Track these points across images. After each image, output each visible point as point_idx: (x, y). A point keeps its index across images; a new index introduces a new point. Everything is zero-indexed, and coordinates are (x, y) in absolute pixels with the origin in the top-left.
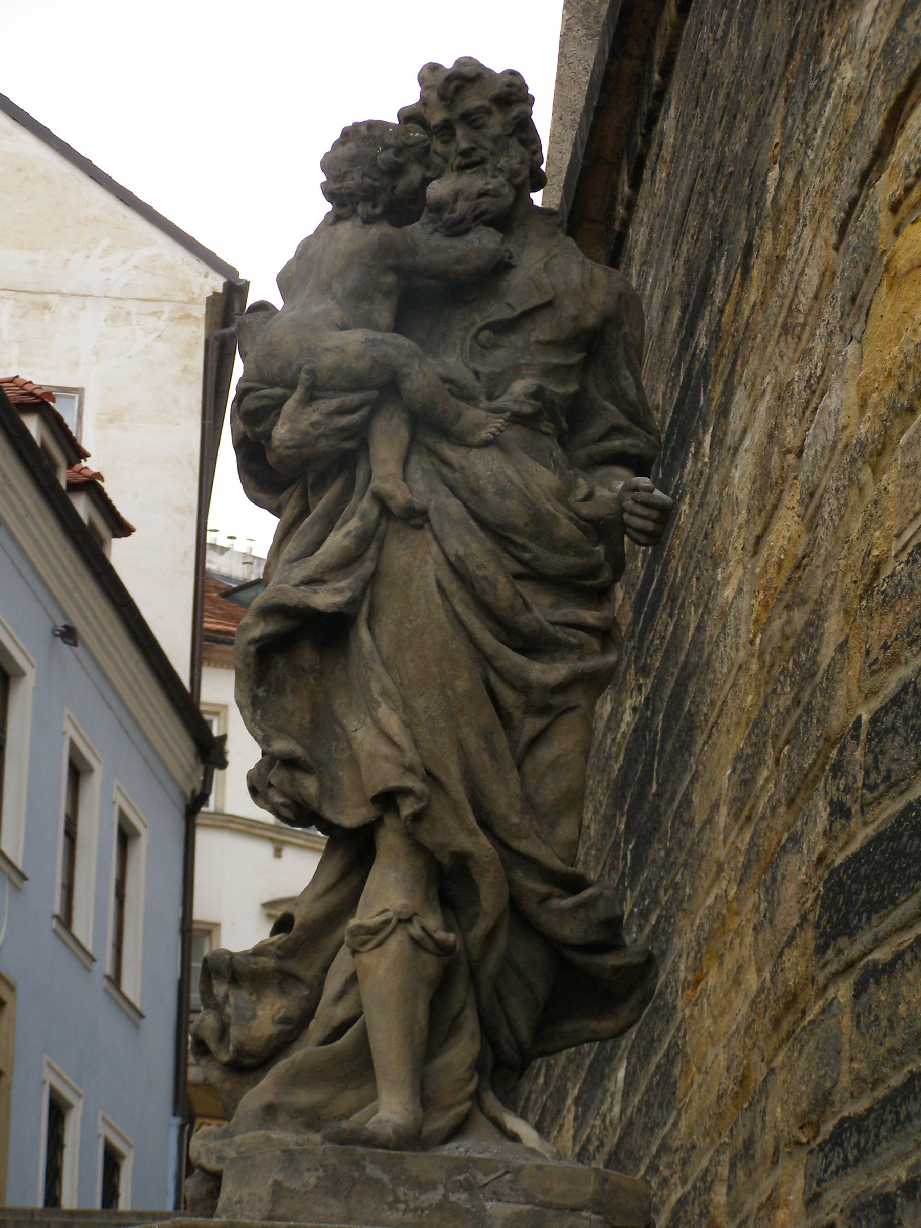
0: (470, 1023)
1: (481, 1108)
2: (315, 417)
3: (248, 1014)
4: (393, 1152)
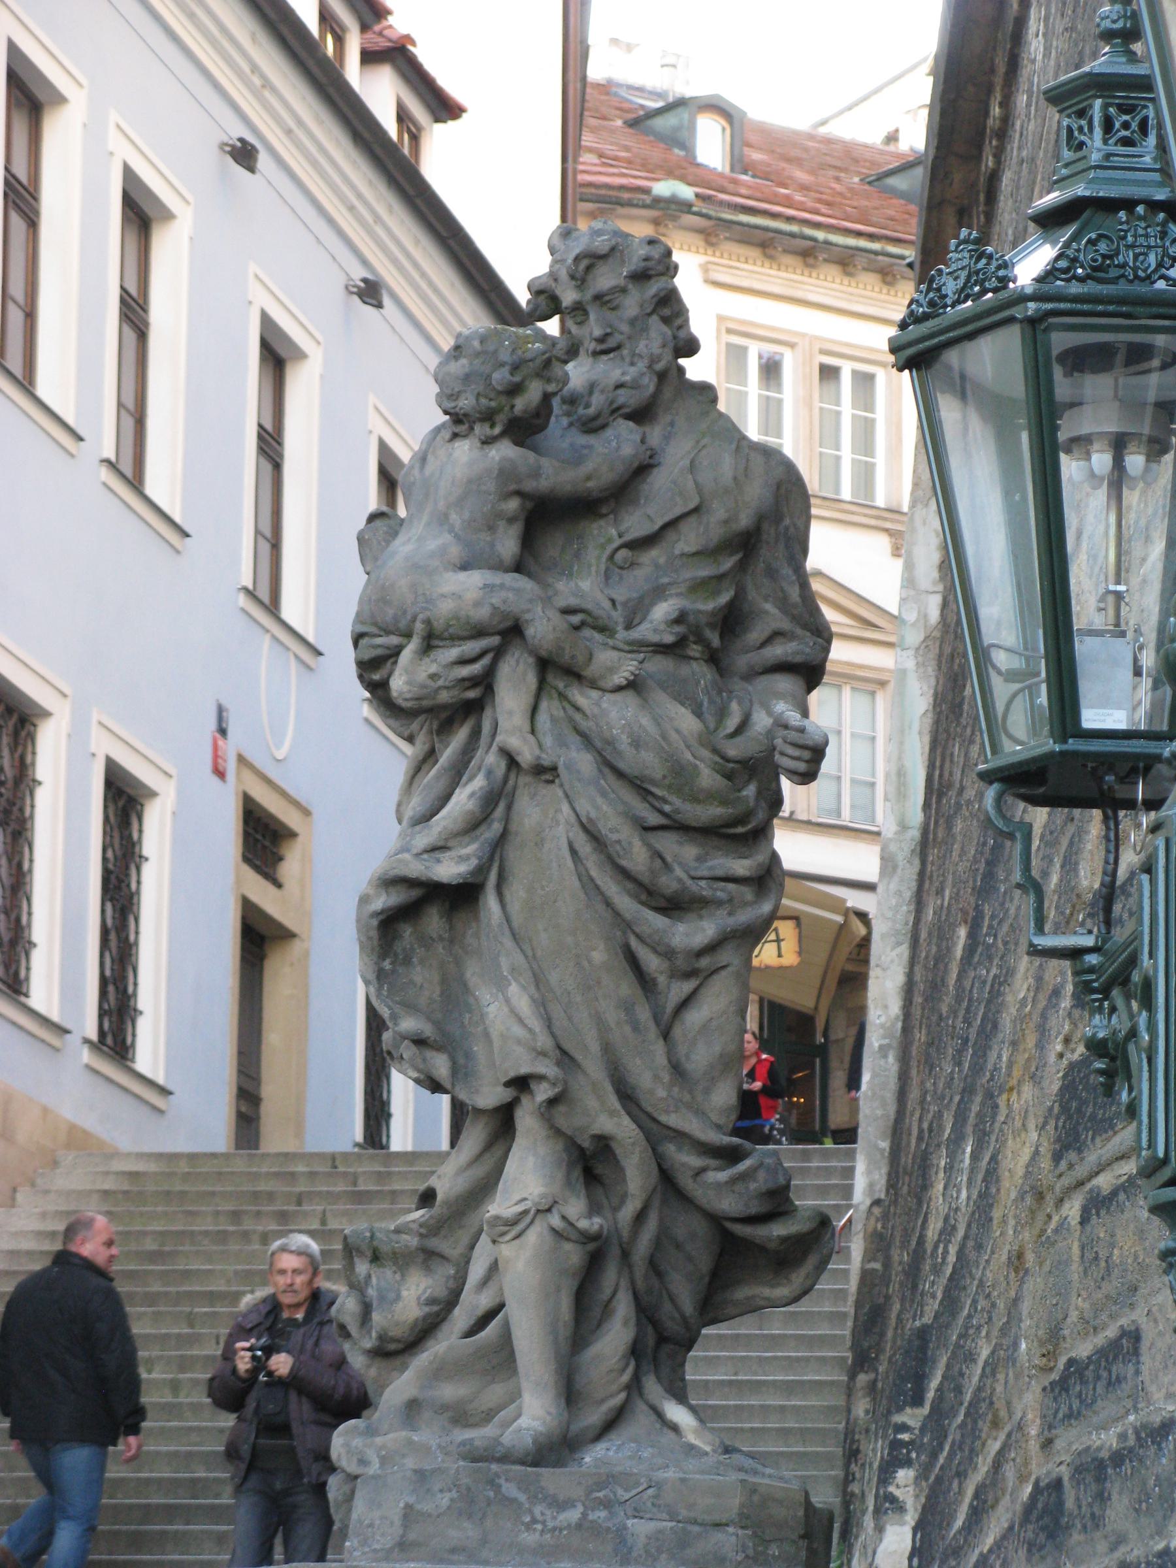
0: (623, 1307)
1: (641, 1394)
2: (433, 668)
3: (392, 1295)
4: (529, 1469)
